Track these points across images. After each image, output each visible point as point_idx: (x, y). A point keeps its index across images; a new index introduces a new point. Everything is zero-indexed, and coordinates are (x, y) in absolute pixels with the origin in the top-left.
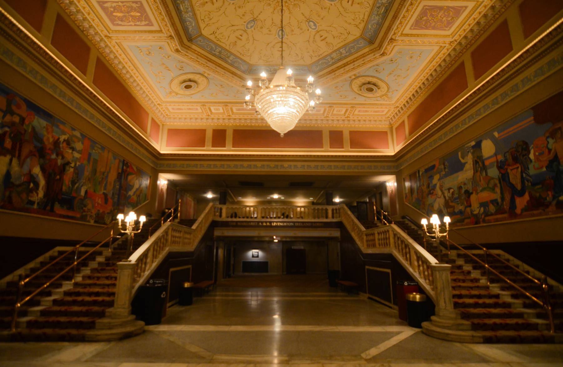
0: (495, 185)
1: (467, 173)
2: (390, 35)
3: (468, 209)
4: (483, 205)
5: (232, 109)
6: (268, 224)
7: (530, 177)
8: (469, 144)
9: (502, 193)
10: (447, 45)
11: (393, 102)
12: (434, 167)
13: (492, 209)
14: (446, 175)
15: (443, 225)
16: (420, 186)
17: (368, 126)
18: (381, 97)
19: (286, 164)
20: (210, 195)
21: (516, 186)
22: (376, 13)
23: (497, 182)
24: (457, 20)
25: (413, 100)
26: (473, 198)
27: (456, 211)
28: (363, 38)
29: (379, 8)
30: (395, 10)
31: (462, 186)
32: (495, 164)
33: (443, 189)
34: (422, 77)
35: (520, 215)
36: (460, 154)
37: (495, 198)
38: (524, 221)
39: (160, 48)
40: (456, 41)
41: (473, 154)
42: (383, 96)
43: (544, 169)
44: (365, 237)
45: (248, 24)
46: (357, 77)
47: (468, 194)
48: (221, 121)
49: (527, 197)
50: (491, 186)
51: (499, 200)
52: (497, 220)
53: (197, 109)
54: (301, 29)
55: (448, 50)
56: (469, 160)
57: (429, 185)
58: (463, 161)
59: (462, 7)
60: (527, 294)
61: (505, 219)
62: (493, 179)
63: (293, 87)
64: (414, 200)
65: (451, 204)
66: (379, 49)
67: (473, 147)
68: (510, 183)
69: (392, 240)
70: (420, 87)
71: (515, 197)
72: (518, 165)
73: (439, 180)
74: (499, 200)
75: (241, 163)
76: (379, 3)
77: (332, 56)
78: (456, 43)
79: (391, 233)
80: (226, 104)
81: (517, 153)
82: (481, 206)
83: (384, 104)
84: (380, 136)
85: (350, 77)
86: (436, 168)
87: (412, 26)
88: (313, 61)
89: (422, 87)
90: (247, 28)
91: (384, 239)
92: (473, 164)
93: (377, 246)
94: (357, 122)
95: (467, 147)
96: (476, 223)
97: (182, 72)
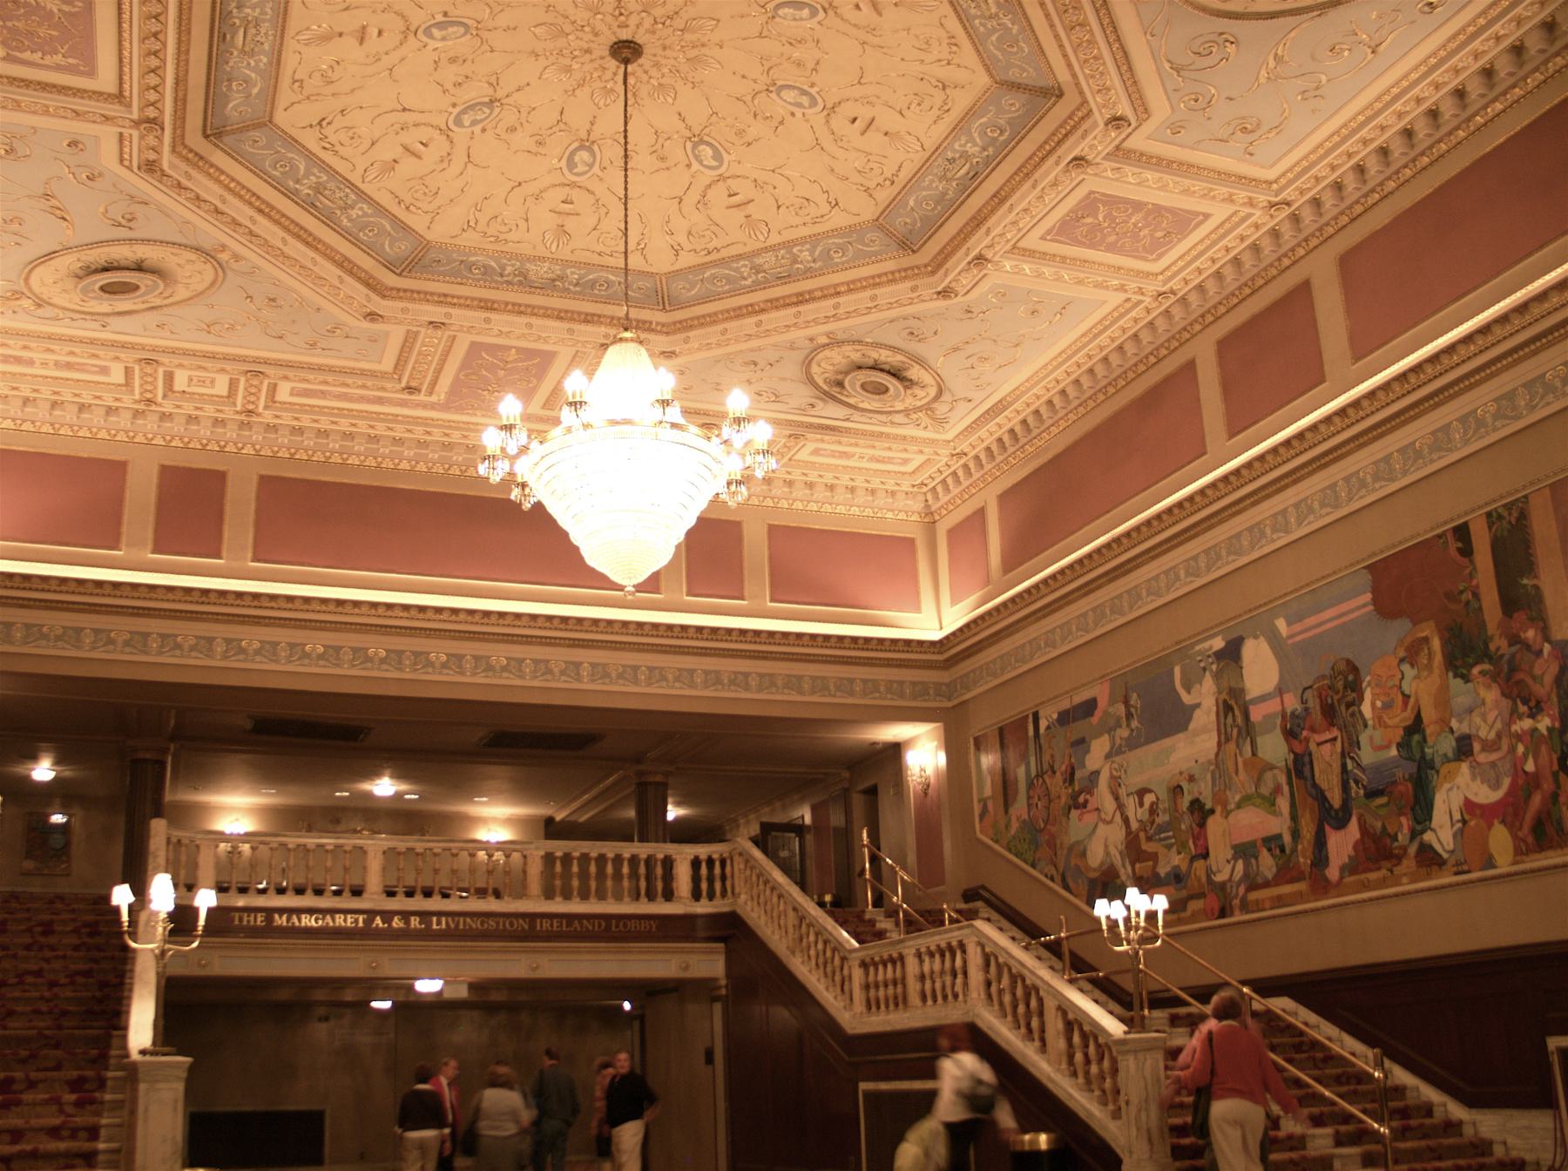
0: (1277, 790)
1: (1195, 746)
2: (978, 243)
3: (1199, 865)
4: (1244, 851)
5: (169, 377)
6: (415, 922)
7: (1363, 770)
8: (1206, 645)
9: (1294, 817)
10: (1148, 300)
11: (950, 436)
12: (1089, 707)
13: (1267, 864)
14: (1133, 744)
15: (182, 918)
16: (1040, 775)
17: (841, 509)
18: (906, 412)
19: (251, 637)
20: (43, 771)
21: (1328, 794)
22: (940, 171)
23: (1283, 779)
24: (1180, 240)
25: (999, 458)
26: (1215, 825)
27: (1163, 870)
28: (881, 228)
29: (952, 161)
30: (1020, 161)
31: (1185, 785)
32: (1279, 721)
33: (1122, 792)
34: (1059, 373)
35: (1339, 887)
36: (1177, 671)
37: (1275, 830)
38: (1346, 904)
39: (73, 144)
40: (1173, 292)
41: (1217, 676)
42: (919, 409)
43: (1394, 752)
44: (857, 974)
45: (464, 112)
46: (835, 342)
47: (1201, 812)
48: (204, 431)
49: (1353, 830)
50: (1265, 790)
51: (1287, 839)
52: (1280, 901)
53: (104, 371)
54: (663, 159)
55: (1148, 311)
56: (1205, 697)
57: (1070, 777)
58: (1187, 699)
59: (1197, 214)
60: (1327, 1093)
61: (1299, 897)
62: (1272, 767)
63: (674, 425)
64: (1015, 826)
65: (1147, 847)
66: (933, 273)
67: (1219, 655)
68: (1315, 785)
69: (976, 976)
70: (1050, 402)
71: (1327, 828)
72: (1335, 732)
73: (1108, 756)
74: (1287, 839)
75: (418, 644)
76: (955, 151)
77: (759, 261)
78: (1173, 299)
79: (975, 957)
80: (255, 370)
81: (1335, 697)
82: (1235, 858)
83: (914, 439)
84: (886, 558)
85: (811, 340)
86: (1098, 713)
87: (1049, 232)
88: (677, 266)
89: (1057, 401)
90: (458, 122)
91: (895, 983)
92: (1218, 713)
93: (914, 999)
94: (800, 492)
95: (1200, 653)
96: (1222, 915)
97: (122, 233)
